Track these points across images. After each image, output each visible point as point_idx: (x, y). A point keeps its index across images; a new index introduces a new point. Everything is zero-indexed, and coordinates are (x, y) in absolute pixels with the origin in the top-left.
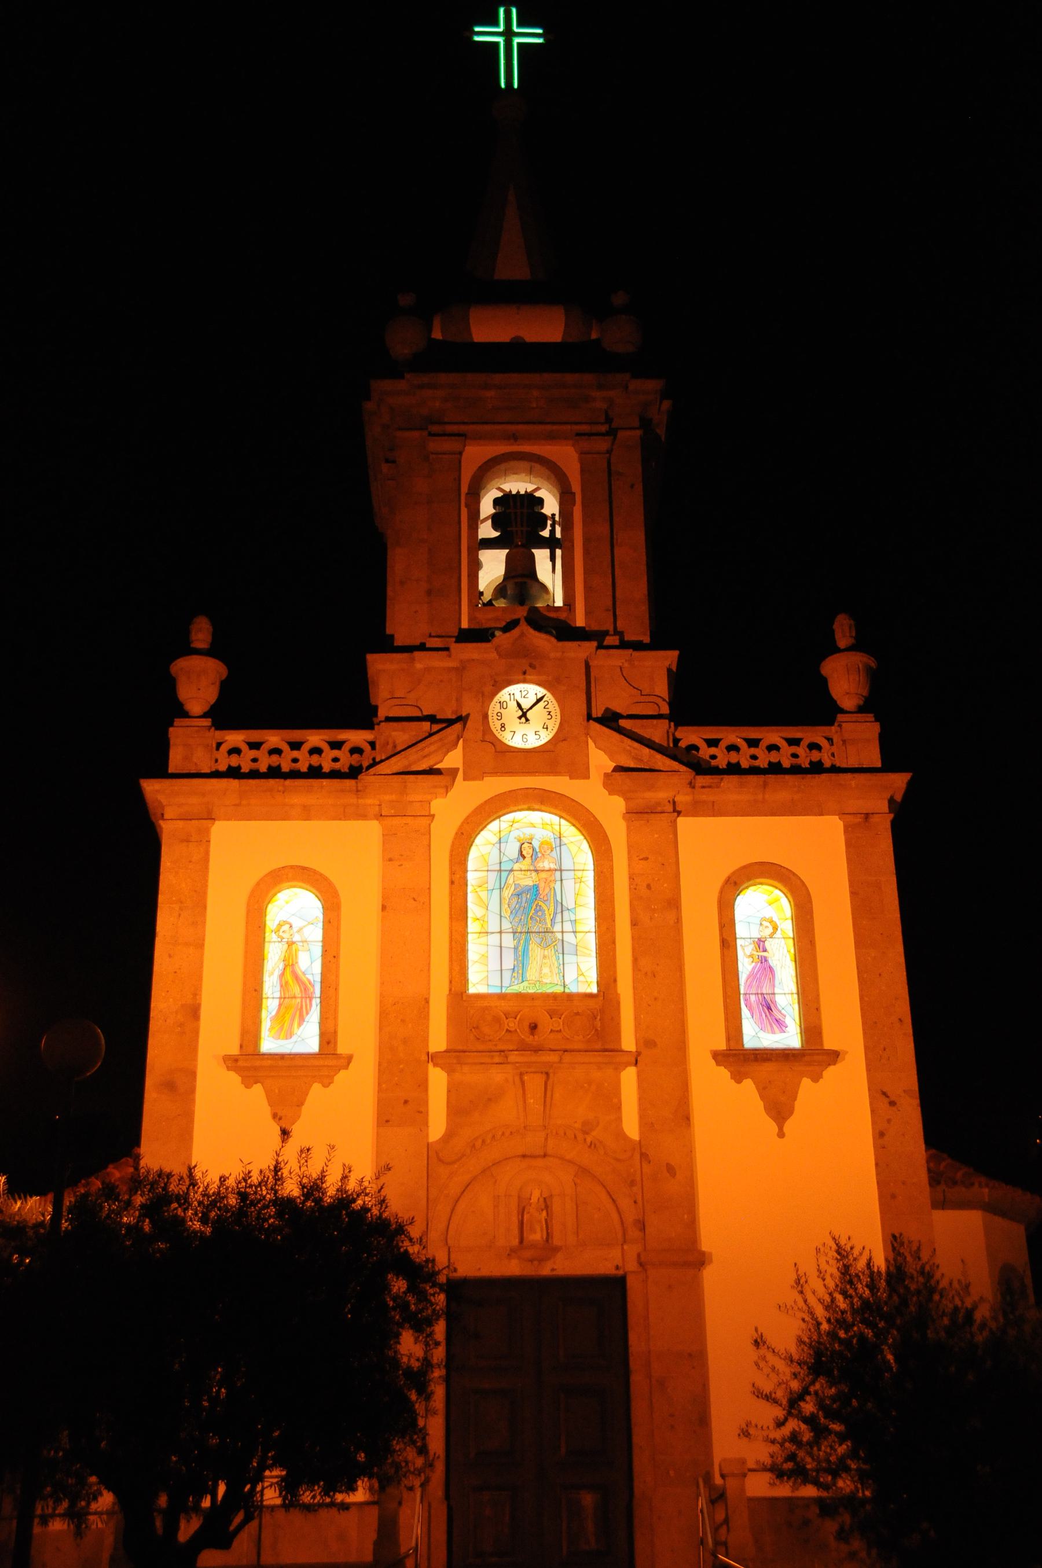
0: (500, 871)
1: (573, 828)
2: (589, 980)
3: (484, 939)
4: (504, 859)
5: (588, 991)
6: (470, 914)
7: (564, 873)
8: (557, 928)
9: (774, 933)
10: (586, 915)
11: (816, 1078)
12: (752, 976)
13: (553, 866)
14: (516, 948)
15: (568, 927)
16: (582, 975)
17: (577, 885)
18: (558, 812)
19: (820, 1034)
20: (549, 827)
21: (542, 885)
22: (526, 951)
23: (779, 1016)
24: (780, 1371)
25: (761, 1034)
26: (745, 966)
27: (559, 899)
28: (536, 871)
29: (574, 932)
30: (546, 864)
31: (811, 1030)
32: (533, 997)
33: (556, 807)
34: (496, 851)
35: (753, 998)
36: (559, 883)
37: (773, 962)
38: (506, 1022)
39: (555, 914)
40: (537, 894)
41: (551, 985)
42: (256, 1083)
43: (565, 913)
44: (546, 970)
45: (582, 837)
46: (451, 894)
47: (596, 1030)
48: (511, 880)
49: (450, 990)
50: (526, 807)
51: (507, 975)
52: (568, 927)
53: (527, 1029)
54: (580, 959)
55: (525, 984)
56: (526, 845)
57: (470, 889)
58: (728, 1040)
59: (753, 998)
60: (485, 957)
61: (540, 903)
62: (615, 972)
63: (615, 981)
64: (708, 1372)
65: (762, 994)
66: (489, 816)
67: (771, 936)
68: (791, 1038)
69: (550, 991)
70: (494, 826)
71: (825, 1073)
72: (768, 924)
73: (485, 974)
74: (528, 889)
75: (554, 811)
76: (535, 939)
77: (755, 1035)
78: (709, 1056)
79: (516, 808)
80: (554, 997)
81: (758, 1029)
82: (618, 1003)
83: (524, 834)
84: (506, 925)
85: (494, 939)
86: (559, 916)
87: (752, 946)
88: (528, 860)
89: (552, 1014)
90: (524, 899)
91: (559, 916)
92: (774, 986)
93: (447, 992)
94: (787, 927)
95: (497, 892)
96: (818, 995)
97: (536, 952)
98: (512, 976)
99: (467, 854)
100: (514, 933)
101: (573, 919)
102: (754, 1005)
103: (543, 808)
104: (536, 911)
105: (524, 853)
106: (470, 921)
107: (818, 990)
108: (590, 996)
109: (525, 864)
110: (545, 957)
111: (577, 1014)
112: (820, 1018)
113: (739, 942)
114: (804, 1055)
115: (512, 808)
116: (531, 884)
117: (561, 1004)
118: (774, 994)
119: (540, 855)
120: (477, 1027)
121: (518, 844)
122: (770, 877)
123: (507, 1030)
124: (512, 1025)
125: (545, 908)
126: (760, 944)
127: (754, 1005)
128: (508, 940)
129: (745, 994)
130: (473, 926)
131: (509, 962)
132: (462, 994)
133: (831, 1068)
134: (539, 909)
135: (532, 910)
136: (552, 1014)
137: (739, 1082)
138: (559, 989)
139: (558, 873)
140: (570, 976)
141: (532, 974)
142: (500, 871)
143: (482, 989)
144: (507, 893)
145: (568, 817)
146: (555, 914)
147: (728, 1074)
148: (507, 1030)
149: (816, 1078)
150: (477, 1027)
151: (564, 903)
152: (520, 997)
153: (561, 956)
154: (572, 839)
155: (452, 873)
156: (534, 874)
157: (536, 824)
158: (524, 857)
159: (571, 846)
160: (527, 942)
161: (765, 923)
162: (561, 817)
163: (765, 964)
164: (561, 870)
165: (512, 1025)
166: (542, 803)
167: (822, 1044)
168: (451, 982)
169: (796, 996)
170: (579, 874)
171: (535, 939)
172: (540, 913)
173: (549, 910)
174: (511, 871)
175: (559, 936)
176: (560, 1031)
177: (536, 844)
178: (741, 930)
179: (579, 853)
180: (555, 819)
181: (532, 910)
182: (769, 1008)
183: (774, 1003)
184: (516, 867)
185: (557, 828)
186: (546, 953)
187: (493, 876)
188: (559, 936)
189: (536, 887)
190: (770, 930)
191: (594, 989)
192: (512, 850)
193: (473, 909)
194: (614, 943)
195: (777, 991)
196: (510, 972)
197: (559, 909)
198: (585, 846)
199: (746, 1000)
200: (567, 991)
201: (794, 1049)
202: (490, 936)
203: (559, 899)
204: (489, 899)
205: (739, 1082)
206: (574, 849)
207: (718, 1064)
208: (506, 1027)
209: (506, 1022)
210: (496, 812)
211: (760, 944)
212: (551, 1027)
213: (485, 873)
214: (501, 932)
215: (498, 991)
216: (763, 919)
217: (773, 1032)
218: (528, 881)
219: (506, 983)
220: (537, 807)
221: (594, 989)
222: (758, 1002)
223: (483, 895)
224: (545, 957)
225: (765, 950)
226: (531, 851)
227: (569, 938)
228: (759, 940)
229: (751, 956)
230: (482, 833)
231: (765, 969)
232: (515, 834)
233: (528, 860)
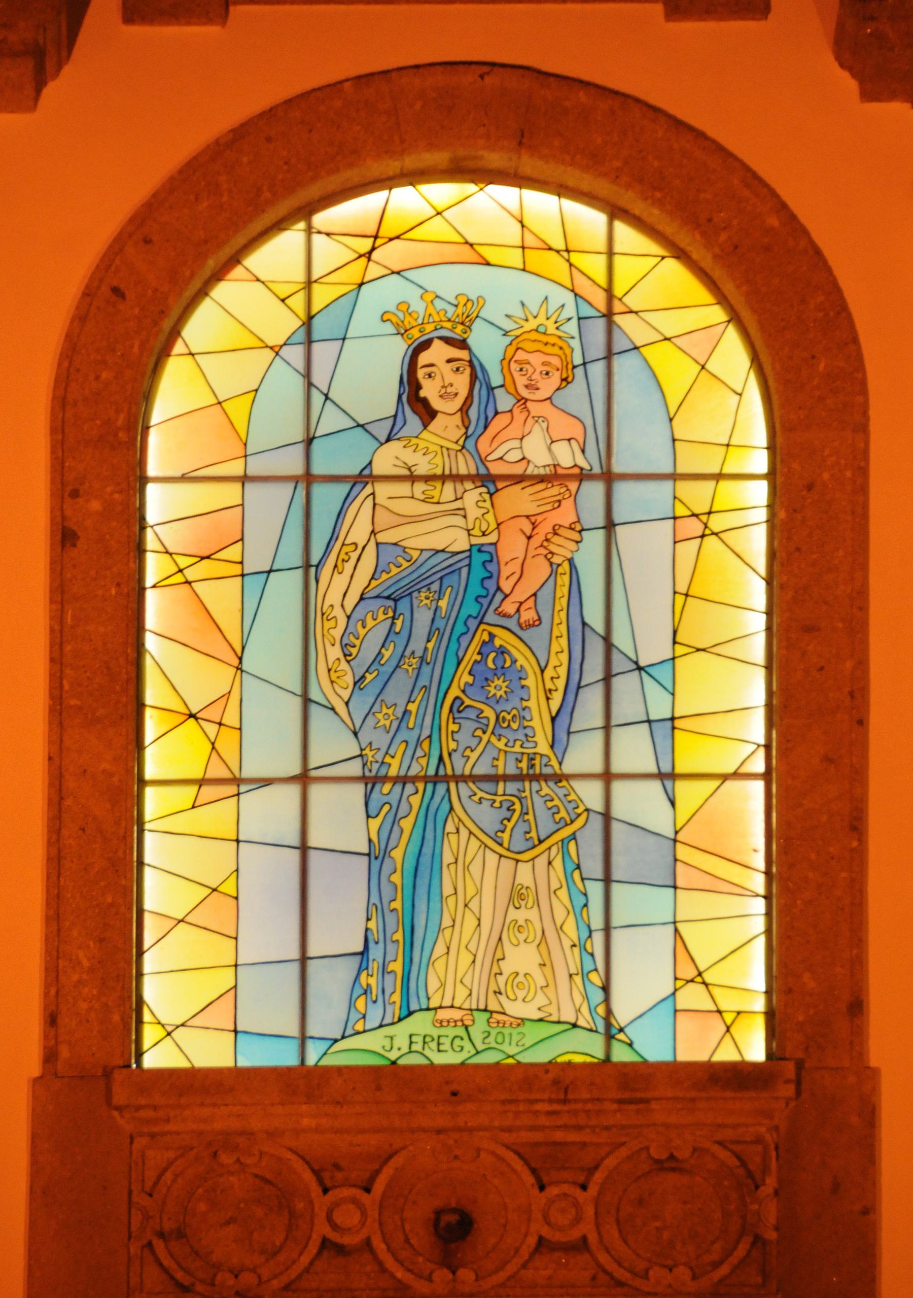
0: (308, 478)
1: (673, 268)
2: (728, 1002)
3: (218, 816)
4: (330, 421)
5: (726, 1054)
6: (154, 692)
7: (622, 490)
8: (584, 755)
10: (729, 700)
13: (566, 456)
14: (376, 856)
15: (634, 751)
16: (698, 978)
17: (687, 550)
18: (603, 187)
20: (556, 266)
21: (512, 548)
22: (425, 867)
27: (595, 617)
28: (487, 480)
29: (667, 777)
30: (537, 448)
32: (454, 1086)
33: (593, 160)
34: (286, 383)
36: (595, 541)
38: (321, 1203)
39: (574, 687)
40: (491, 590)
41: (544, 1025)
42: (869, 1068)
43: (625, 686)
44: (521, 958)
45: (718, 314)
46: (60, 592)
47: (758, 1240)
48: (358, 530)
49: (50, 1057)
50: (440, 158)
51: (331, 985)
52: (634, 751)
53: (421, 1238)
54: (691, 904)
55: (420, 1024)
56: (438, 353)
57: (155, 567)
60: (223, 895)
61: (503, 638)
62: (857, 965)
63: (857, 1007)
66: (257, 207)
69: (540, 1056)
70: (279, 255)
73: (226, 979)
74: (445, 570)
75: (587, 181)
76: (476, 809)
78: (543, 1193)
79: (393, 166)
80: (559, 1080)
82: (870, 1115)
83: (431, 297)
84: (332, 744)
85: (270, 813)
86: (592, 700)
88: (447, 427)
89: (544, 1164)
90: (423, 618)
91: (592, 700)
93: (35, 1069)
95: (286, 587)
97: (475, 875)
98: (358, 990)
99: (148, 397)
100: (371, 781)
101: (660, 709)
103: (528, 164)
104: (481, 679)
105: (429, 390)
106: (152, 725)
108: (737, 1076)
109: (430, 447)
110: (517, 896)
111: (670, 1164)
115: (376, 168)
116: (462, 544)
117: (602, 1110)
119: (504, 401)
120: (180, 1234)
121: (398, 349)
123: (325, 1243)
124: (353, 1219)
125: (523, 659)
128: (340, 816)
130: (167, 751)
131: (340, 925)
132: (108, 1074)
134: (495, 664)
135: (462, 677)
136: (544, 1164)
138: (584, 1048)
139: (594, 492)
140: (640, 979)
141: (451, 976)
142: (308, 478)
143: (210, 1052)
144: (338, 589)
145: (654, 214)
146: (574, 687)
148: (325, 1243)
150: (180, 1234)
151: (620, 638)
152: (391, 1081)
153: (595, 890)
154: (671, 324)
155: (66, 489)
156: (473, 496)
157: (492, 239)
158: (427, 413)
159: (663, 358)
160: (432, 825)
162: (616, 212)
164: (609, 478)
165: (348, 1217)
166: (523, 140)
168: (52, 1020)
170: (696, 495)
171: (476, 809)
172: (498, 688)
173: (541, 666)
174: (364, 478)
175: (590, 794)
176: (582, 1245)
177: (487, 346)
179: (706, 395)
180: (588, 220)
181: (462, 677)
184: (387, 460)
185: (596, 266)
186: (524, 874)
187: (270, 506)
188: (590, 794)
189: (486, 556)
191: (755, 1050)
192: (368, 374)
193: (172, 670)
194: (857, 824)
196: (346, 970)
197: (594, 669)
198: (733, 356)
200: (621, 1054)
202: (253, 800)
203: (595, 617)
204: (248, 622)
206: (675, 370)
208: (322, 1229)
209: (321, 1203)
210: (290, 189)
212: (539, 1228)
213: (230, 494)
214: (304, 779)
215: (284, 1056)
218: (441, 530)
219: (325, 1019)
220: (495, 159)
221: (755, 1050)
223: (222, 598)
224: (517, 896)
226: (461, 383)
227: (640, 803)
230: (222, 291)
232: (384, 294)
233: (447, 427)
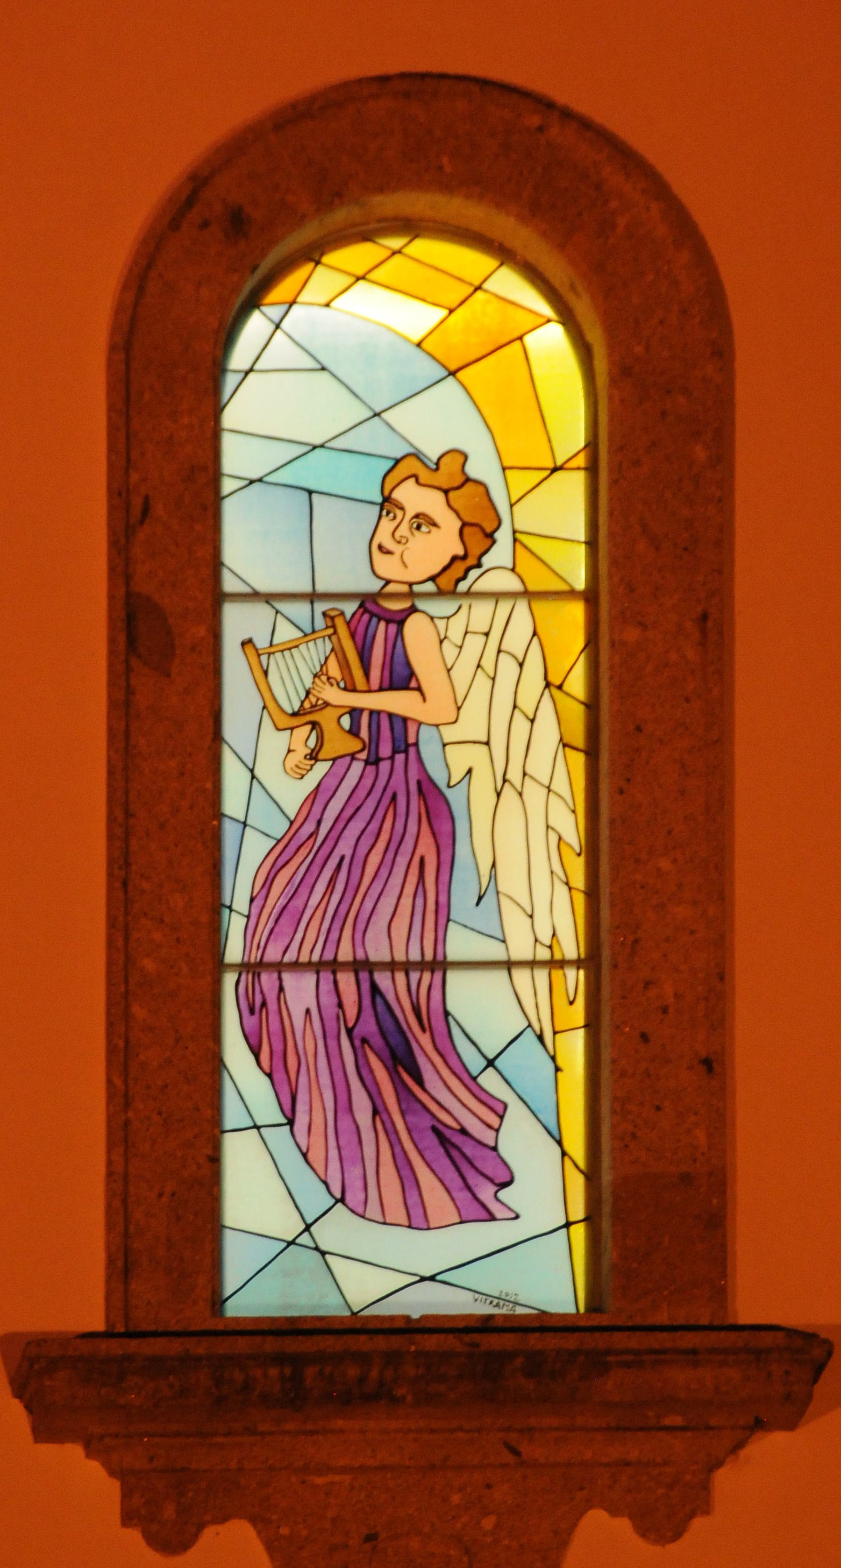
9: (466, 562)
11: (666, 1513)
12: (303, 844)
19: (715, 1222)
23: (462, 1112)
24: (327, 686)
25: (340, 1231)
26: (265, 780)
31: (655, 1191)
35: (301, 992)
37: (451, 758)
58: (123, 1266)
59: (301, 992)
64: (109, 536)
65: (362, 966)
67: (452, 579)
68: (529, 1252)
71: (725, 1481)
72: (430, 502)
77: (292, 1227)
81: (315, 1198)
87: (316, 651)
92: (443, 915)
94: (555, 522)
96: (722, 974)
102: (308, 1040)
107: (720, 942)
112: (720, 1123)
113: (238, 623)
114: (598, 1363)
118: (439, 965)
122: (472, 182)
126: (371, 631)
127: (308, 1040)
129: (252, 968)
133: (777, 1439)
137: (172, 1540)
147: (109, 1490)
149: (666, 1513)
161: (413, 498)
163: (394, 774)
167: (721, 1294)
169: (575, 979)
178: (253, 545)
182: (402, 1061)
183: (439, 1022)
190: (442, 544)
195: (460, 944)
199: (253, 1008)
201: (543, 1324)
205: (172, 1540)
207: (47, 1427)
211: (371, 631)
216: (407, 465)
217: (417, 1219)
222: (335, 1025)
225: (402, 677)
228: (369, 604)
229: (308, 714)
231: (393, 797)
